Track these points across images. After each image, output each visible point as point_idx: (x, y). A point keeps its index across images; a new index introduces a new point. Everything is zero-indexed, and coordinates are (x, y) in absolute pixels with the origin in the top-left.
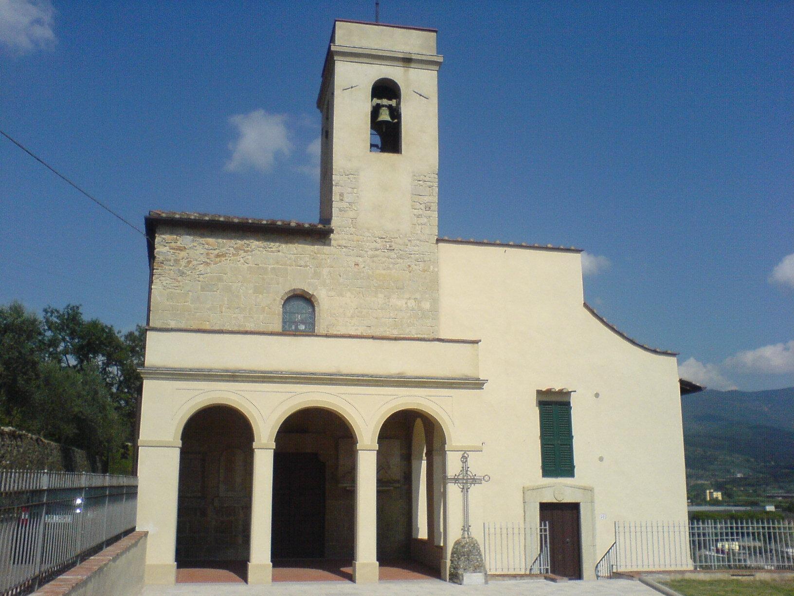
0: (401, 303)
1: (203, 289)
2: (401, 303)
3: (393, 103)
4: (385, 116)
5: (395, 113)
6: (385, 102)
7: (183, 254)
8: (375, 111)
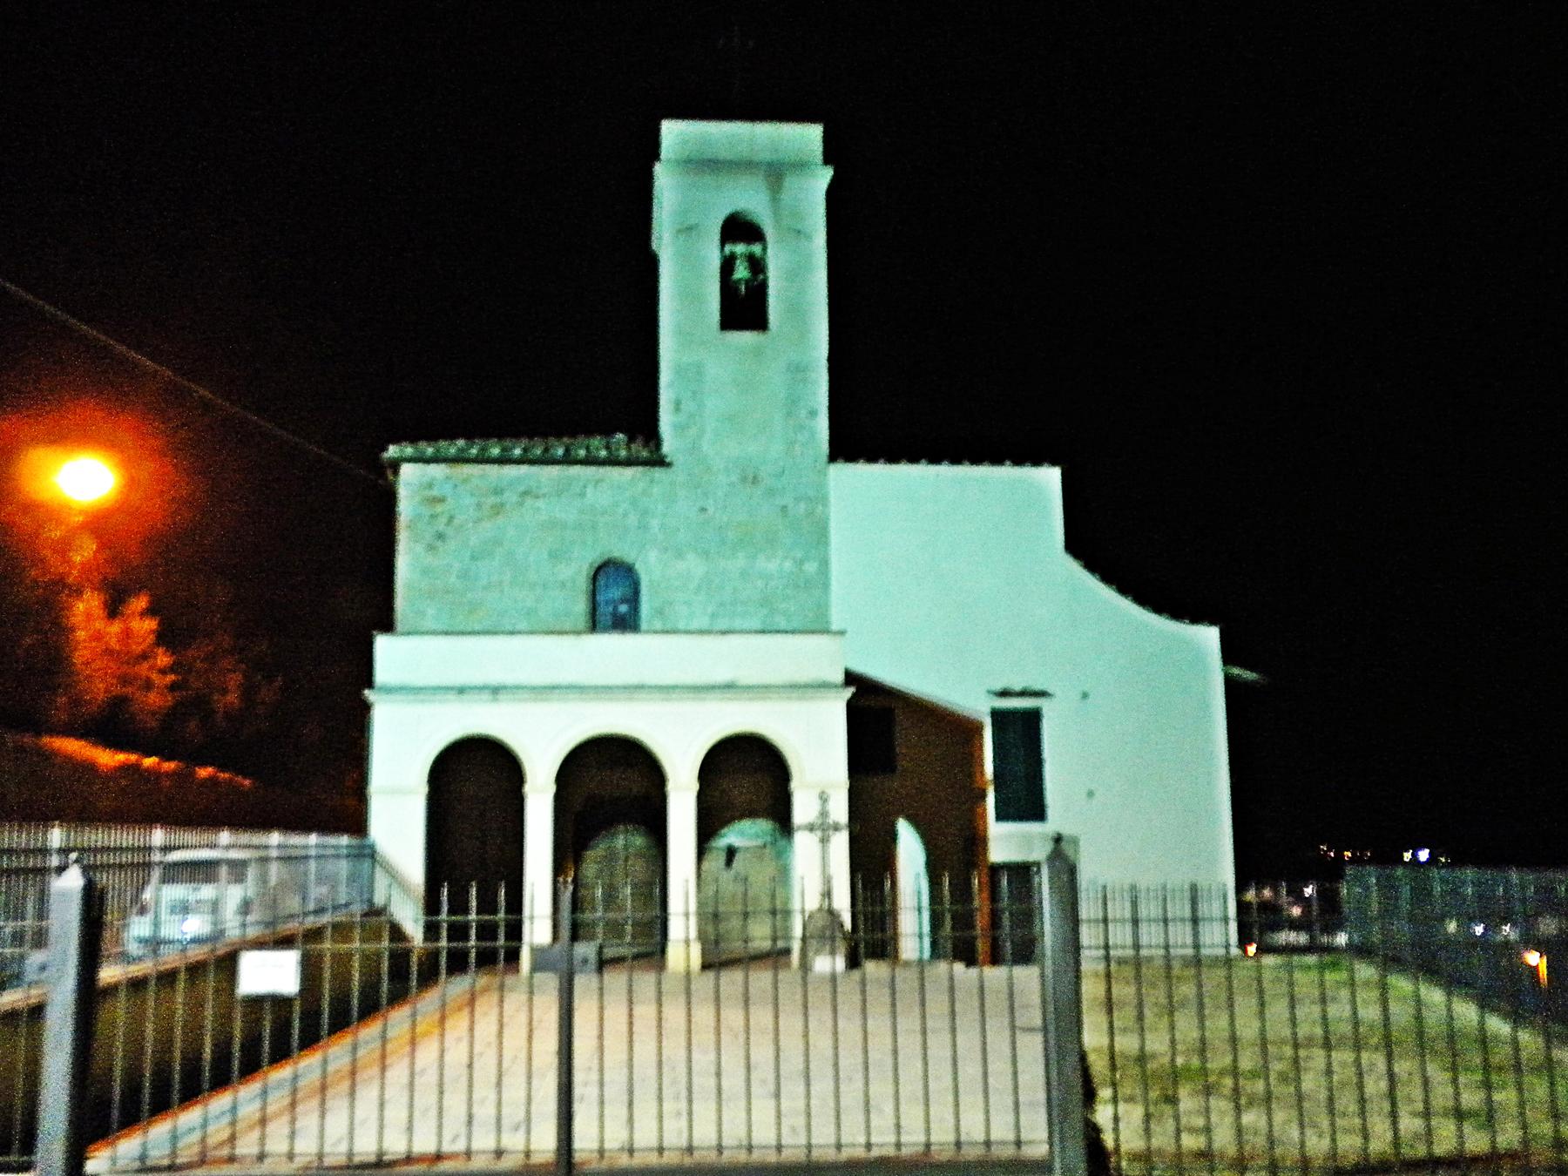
0: (772, 566)
1: (473, 558)
2: (772, 566)
3: (756, 249)
4: (741, 272)
5: (757, 265)
6: (740, 248)
7: (439, 508)
8: (728, 265)
